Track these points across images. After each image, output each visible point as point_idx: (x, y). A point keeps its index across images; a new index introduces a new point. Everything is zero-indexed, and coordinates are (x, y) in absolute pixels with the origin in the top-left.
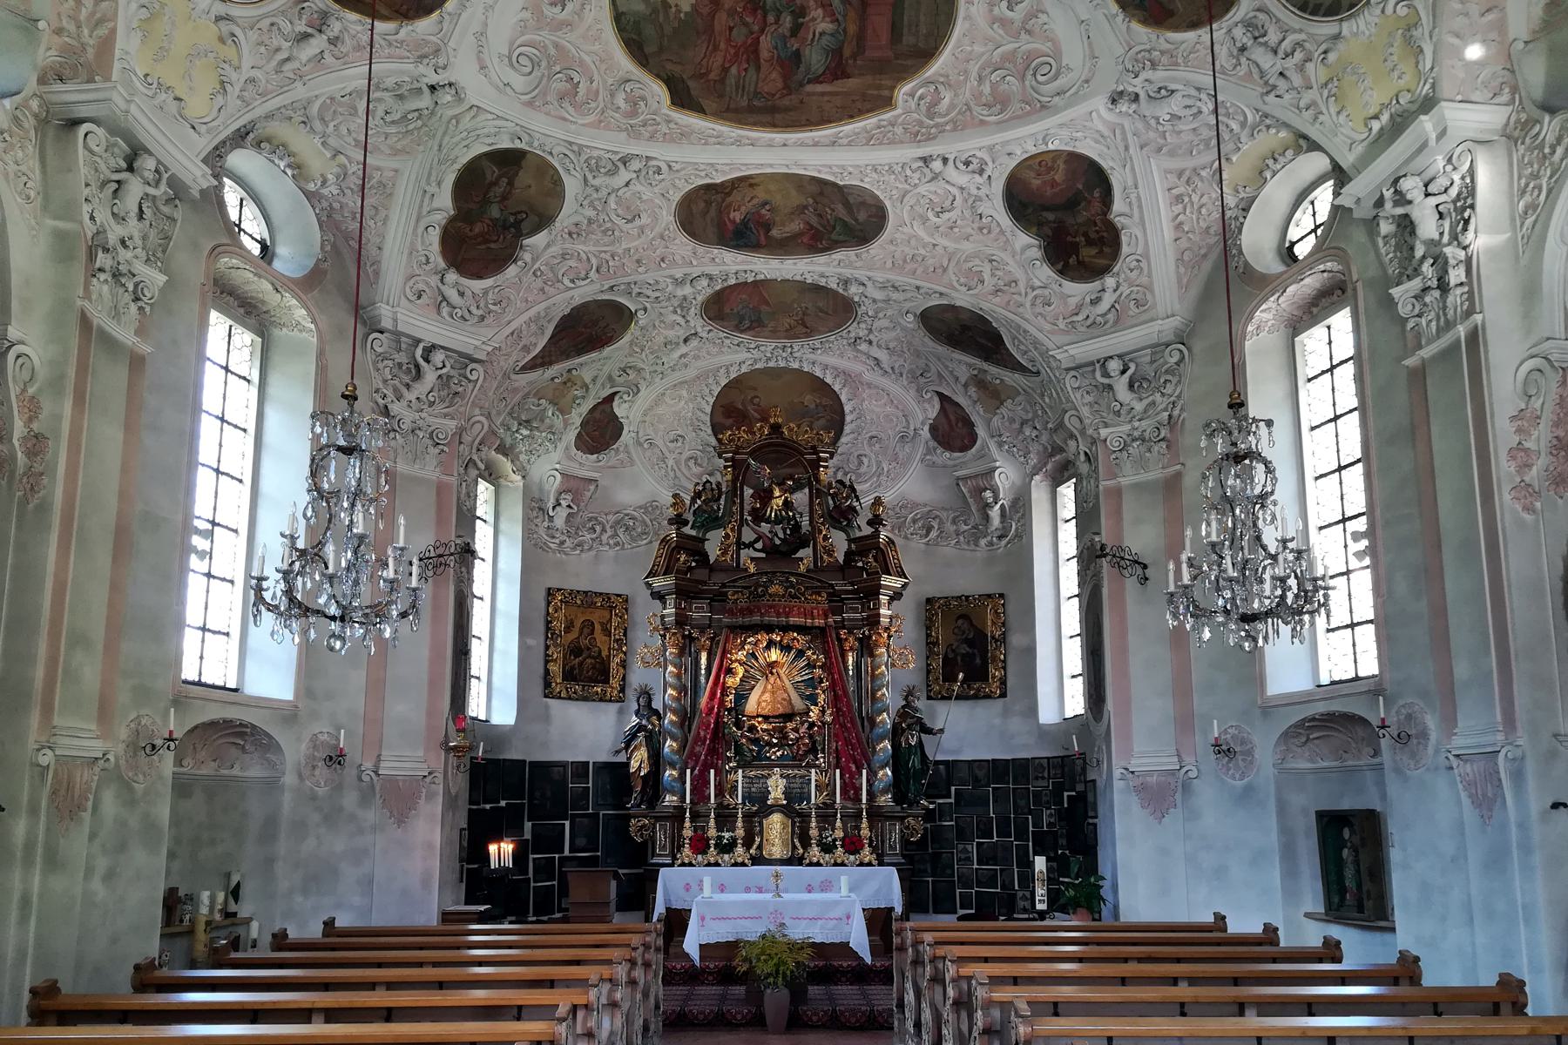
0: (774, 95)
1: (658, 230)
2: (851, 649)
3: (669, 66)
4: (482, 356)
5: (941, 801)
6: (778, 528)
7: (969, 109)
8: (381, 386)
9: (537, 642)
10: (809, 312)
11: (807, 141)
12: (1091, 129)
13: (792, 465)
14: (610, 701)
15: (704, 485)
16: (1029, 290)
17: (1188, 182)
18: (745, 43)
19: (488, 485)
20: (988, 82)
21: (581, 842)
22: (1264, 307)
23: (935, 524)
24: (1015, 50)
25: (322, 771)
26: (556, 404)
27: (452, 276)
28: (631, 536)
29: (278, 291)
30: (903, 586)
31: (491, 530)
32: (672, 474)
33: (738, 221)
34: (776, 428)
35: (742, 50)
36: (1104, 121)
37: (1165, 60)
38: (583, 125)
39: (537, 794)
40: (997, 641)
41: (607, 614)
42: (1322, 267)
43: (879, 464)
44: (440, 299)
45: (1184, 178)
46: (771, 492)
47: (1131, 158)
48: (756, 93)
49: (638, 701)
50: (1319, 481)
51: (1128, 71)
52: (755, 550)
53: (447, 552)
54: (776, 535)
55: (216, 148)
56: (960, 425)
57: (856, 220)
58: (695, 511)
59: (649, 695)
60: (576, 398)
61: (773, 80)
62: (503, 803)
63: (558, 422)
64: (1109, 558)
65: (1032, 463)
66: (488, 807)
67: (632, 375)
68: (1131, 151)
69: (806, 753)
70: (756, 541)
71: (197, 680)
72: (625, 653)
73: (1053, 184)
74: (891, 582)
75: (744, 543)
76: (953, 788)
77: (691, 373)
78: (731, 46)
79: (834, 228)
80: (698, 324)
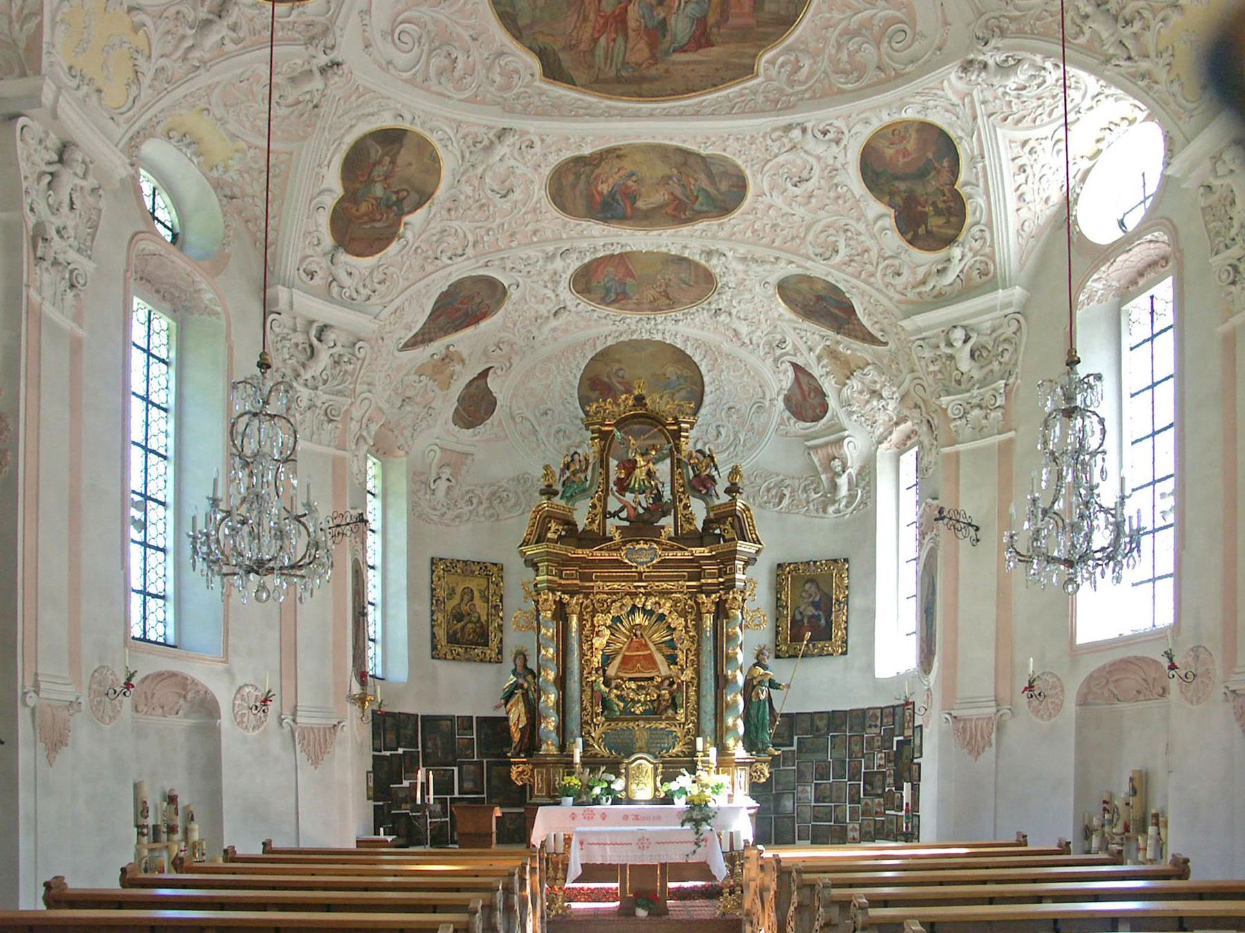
0: (641, 65)
1: (530, 205)
2: (708, 612)
3: (541, 38)
5: (783, 749)
7: (827, 75)
9: (425, 608)
10: (672, 284)
11: (673, 111)
12: (941, 97)
13: (654, 437)
14: (490, 662)
15: (572, 456)
17: (1030, 152)
18: (614, 12)
19: (375, 460)
20: (845, 52)
21: (468, 785)
22: (1095, 276)
23: (787, 492)
24: (872, 17)
30: (757, 552)
33: (605, 192)
34: (640, 400)
35: (610, 20)
36: (956, 92)
37: (1013, 27)
38: (460, 100)
39: (429, 744)
41: (484, 582)
42: (1149, 237)
43: (736, 434)
44: (330, 279)
45: (1027, 148)
47: (979, 129)
48: (625, 64)
49: (515, 661)
50: (1135, 445)
51: (979, 38)
53: (344, 523)
55: (132, 138)
56: (812, 395)
57: (718, 190)
58: (564, 482)
59: (525, 656)
61: (640, 51)
62: (400, 751)
64: (946, 520)
65: (878, 433)
66: (388, 753)
68: (979, 120)
70: (621, 510)
72: (502, 619)
73: (906, 153)
74: (744, 547)
75: (609, 513)
76: (795, 738)
78: (602, 17)
79: (697, 197)
80: (567, 296)
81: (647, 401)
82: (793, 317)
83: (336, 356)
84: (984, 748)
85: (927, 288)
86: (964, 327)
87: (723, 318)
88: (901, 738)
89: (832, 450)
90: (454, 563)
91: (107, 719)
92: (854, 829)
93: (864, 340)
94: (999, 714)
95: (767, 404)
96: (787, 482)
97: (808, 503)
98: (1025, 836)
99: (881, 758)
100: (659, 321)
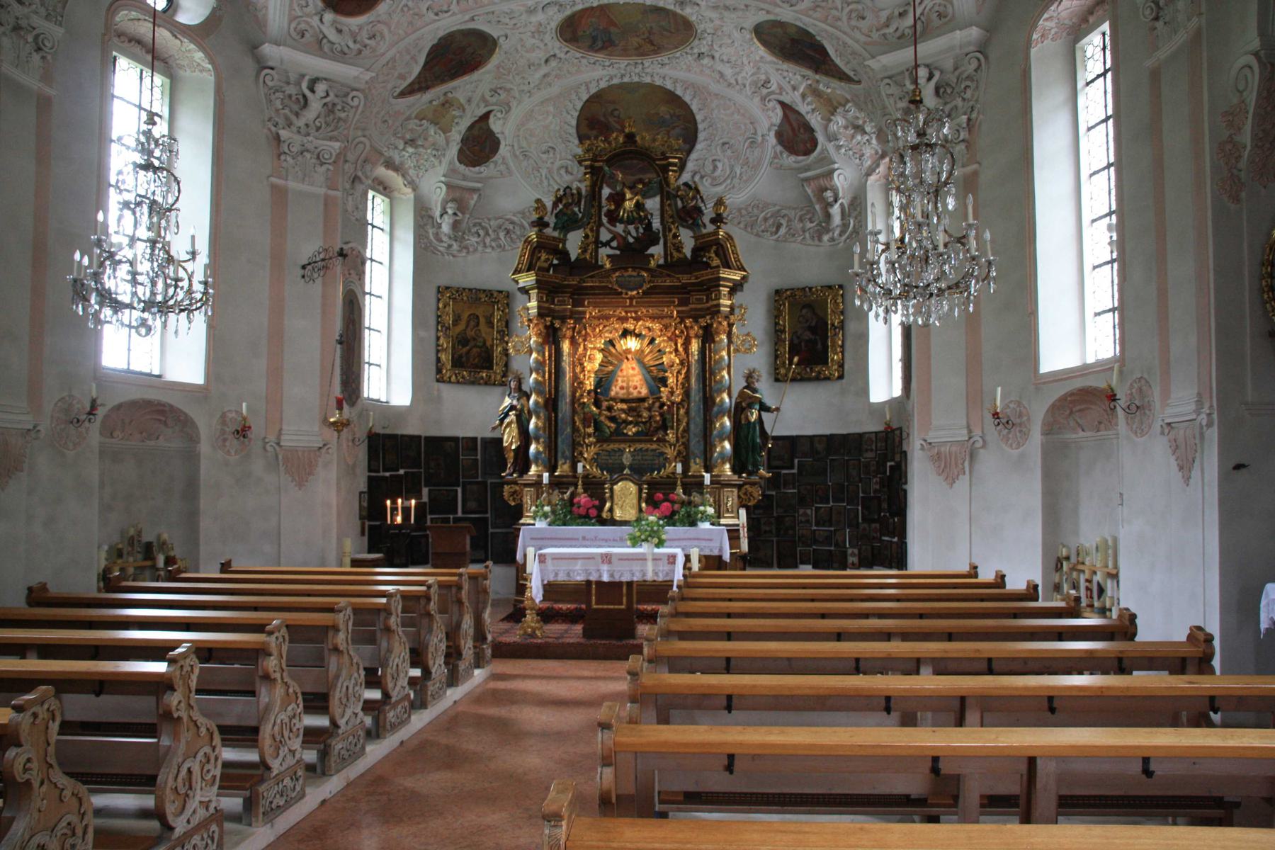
4: (362, 86)
6: (631, 228)
8: (273, 115)
9: (430, 334)
14: (494, 384)
16: (845, 5)
21: (472, 505)
22: (1046, 16)
23: (784, 222)
25: (233, 443)
26: (436, 124)
27: (329, 16)
28: (511, 238)
29: (176, 37)
31: (386, 238)
32: (546, 183)
40: (836, 328)
44: (321, 36)
46: (624, 195)
52: (612, 248)
54: (629, 233)
56: (802, 131)
60: (455, 117)
62: (402, 472)
63: (440, 139)
66: (387, 474)
67: (503, 96)
69: (657, 429)
70: (612, 240)
71: (126, 367)
75: (601, 242)
76: (796, 461)
77: (555, 89)
80: (556, 46)
81: (638, 138)
82: (774, 59)
83: (330, 105)
84: (958, 475)
85: (891, 30)
86: (927, 66)
87: (706, 61)
88: (893, 463)
89: (822, 182)
90: (461, 291)
91: (71, 445)
92: (853, 554)
93: (841, 79)
94: (972, 441)
95: (760, 139)
96: (784, 212)
97: (804, 232)
98: (976, 568)
99: (876, 483)
100: (647, 64)
